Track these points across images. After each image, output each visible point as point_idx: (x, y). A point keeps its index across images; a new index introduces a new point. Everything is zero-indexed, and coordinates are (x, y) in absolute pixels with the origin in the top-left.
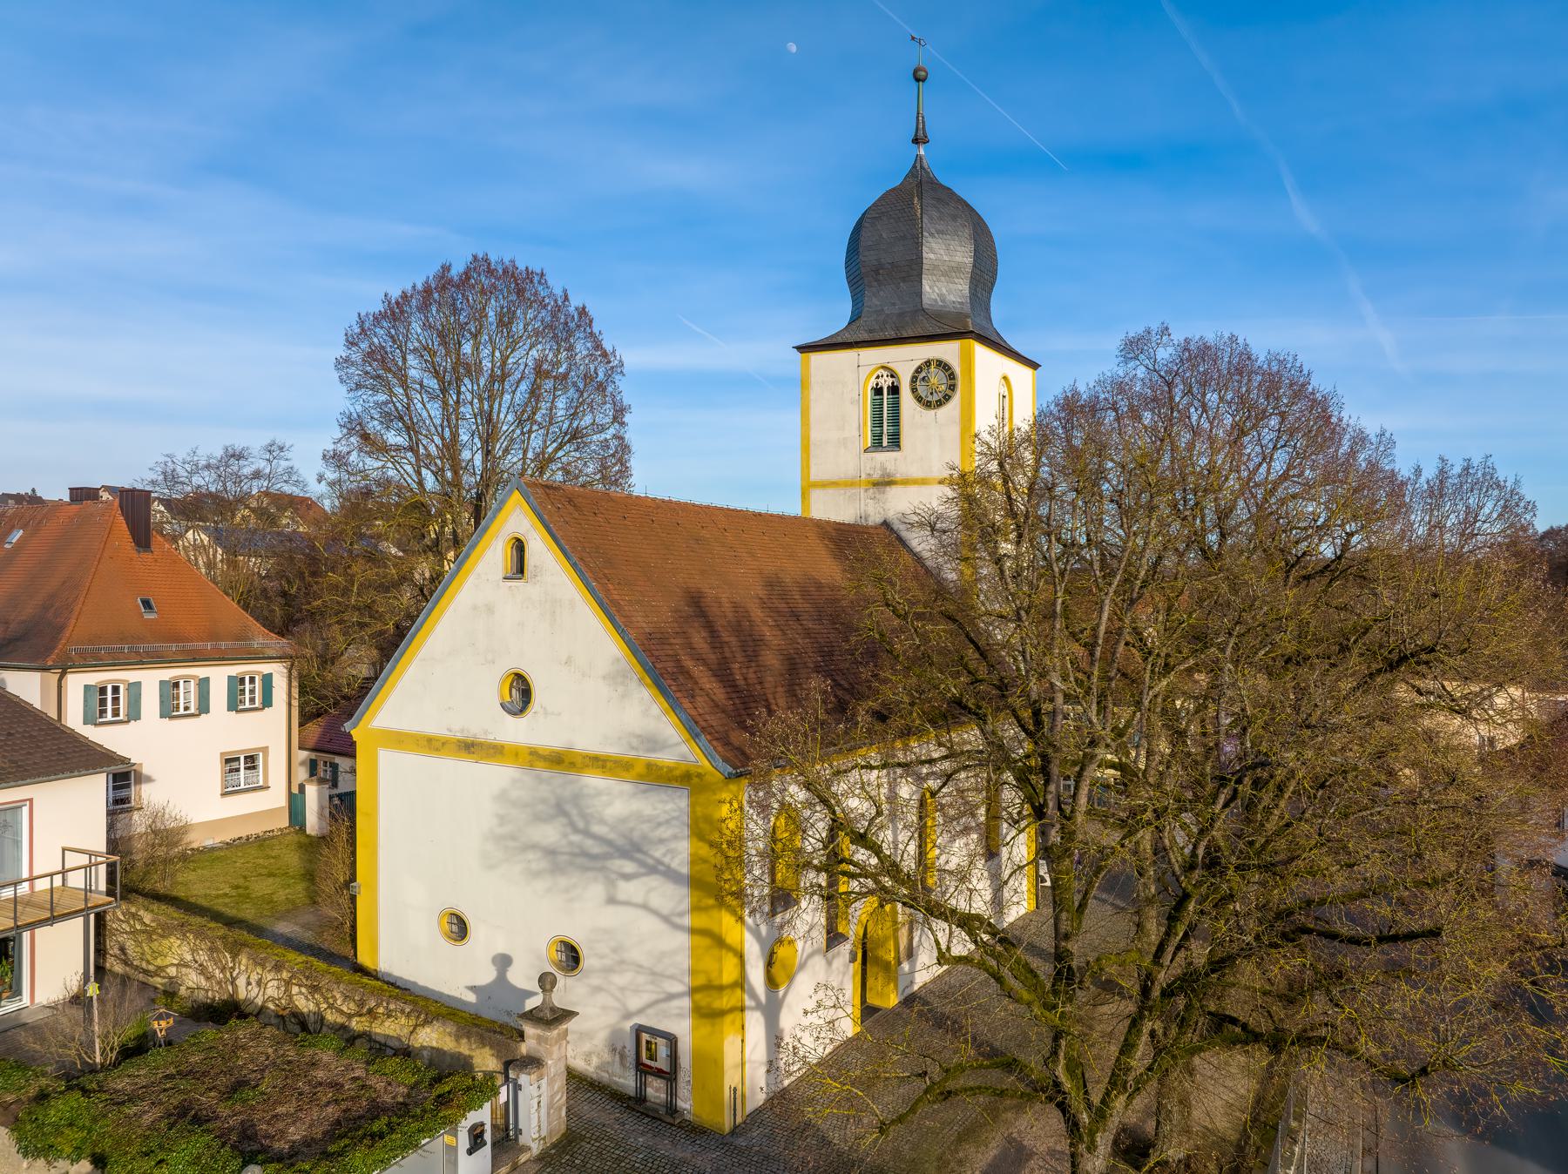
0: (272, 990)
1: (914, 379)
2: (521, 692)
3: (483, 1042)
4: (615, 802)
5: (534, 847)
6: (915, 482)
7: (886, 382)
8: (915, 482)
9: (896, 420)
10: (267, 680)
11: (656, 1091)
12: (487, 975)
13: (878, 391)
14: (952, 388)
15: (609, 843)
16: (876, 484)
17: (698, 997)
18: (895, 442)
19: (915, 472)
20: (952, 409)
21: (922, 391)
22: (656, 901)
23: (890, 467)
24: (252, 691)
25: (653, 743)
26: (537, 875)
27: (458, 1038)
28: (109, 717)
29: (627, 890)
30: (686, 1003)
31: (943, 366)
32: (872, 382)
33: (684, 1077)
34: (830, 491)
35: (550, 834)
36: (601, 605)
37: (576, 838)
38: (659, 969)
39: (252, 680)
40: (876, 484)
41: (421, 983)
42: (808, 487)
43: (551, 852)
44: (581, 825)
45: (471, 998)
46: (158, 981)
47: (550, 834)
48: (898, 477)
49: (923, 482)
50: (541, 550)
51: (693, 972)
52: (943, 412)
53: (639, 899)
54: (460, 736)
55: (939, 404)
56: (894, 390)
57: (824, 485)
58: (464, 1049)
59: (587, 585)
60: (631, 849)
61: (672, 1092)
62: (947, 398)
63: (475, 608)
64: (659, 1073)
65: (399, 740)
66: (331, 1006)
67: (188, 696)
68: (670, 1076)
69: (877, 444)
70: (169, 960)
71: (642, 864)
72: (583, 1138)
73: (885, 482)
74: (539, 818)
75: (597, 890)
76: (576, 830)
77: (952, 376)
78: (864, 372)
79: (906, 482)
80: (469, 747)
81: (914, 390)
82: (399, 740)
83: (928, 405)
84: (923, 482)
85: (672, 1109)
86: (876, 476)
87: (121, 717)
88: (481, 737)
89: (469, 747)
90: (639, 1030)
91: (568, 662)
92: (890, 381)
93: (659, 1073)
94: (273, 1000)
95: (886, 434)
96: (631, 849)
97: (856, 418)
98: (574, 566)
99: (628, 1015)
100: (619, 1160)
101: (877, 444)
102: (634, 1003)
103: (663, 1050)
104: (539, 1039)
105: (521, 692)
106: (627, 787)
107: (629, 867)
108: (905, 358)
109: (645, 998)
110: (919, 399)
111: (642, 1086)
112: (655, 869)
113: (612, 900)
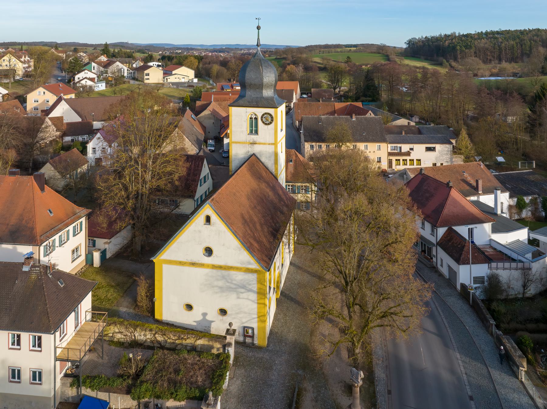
0: (149, 336)
1: (262, 117)
2: (209, 251)
3: (216, 341)
4: (239, 277)
5: (217, 286)
6: (262, 144)
7: (254, 117)
8: (262, 144)
9: (257, 126)
11: (248, 340)
12: (200, 318)
13: (251, 118)
14: (272, 120)
15: (238, 285)
16: (251, 144)
17: (261, 318)
18: (256, 132)
19: (262, 141)
20: (272, 125)
21: (264, 120)
22: (250, 298)
23: (255, 139)
25: (249, 263)
26: (217, 293)
27: (209, 341)
29: (242, 295)
30: (256, 320)
32: (250, 116)
33: (255, 336)
34: (238, 144)
35: (220, 283)
36: (233, 233)
37: (228, 284)
40: (251, 144)
41: (178, 321)
43: (221, 288)
44: (230, 281)
45: (195, 324)
46: (107, 338)
47: (220, 283)
48: (257, 142)
49: (265, 144)
50: (214, 218)
51: (258, 313)
52: (269, 126)
53: (246, 297)
54: (190, 261)
55: (269, 124)
56: (256, 119)
57: (236, 143)
58: (211, 343)
59: (229, 228)
60: (243, 287)
61: (253, 340)
62: (271, 123)
63: (195, 231)
64: (250, 336)
65: (170, 262)
66: (169, 338)
67: (64, 238)
68: (252, 337)
69: (251, 132)
70: (109, 332)
71: (246, 289)
72: (239, 357)
73: (254, 143)
74: (218, 280)
75: (234, 296)
76: (228, 282)
77: (272, 118)
78: (248, 114)
79: (260, 144)
80: (193, 264)
81: (262, 120)
82: (170, 262)
83: (266, 124)
84: (265, 144)
85: (253, 344)
86: (251, 141)
88: (197, 262)
89: (193, 264)
90: (244, 327)
91: (223, 245)
93: (250, 336)
94: (149, 339)
95: (254, 130)
96: (243, 287)
97: (246, 126)
98: (226, 224)
99: (243, 323)
100: (249, 361)
102: (244, 320)
103: (250, 331)
104: (230, 338)
105: (209, 251)
106: (242, 273)
107: (243, 290)
108: (260, 112)
109: (247, 319)
110: (263, 122)
111: (245, 339)
112: (250, 290)
113: (238, 298)
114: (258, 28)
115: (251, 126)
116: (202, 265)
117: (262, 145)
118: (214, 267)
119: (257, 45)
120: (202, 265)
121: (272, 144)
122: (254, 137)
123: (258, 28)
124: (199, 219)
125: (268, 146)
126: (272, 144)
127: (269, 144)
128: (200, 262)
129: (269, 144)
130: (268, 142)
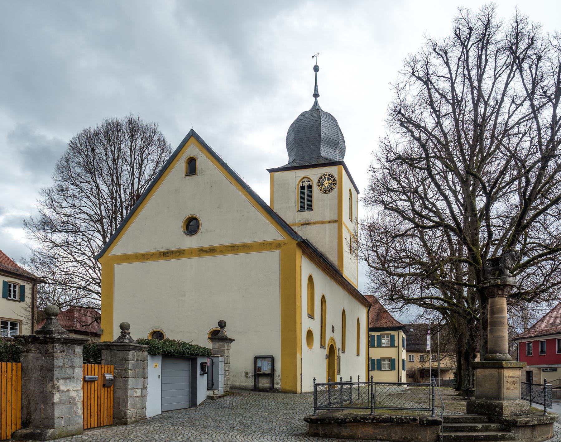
7: (306, 184)
9: (310, 199)
10: (22, 288)
13: (303, 188)
18: (310, 208)
19: (319, 219)
20: (334, 193)
24: (15, 292)
28: (12, 298)
31: (331, 177)
32: (301, 184)
38: (433, 79)
39: (15, 287)
42: (316, 408)
49: (323, 223)
52: (330, 195)
56: (310, 187)
61: (272, 382)
65: (126, 259)
68: (271, 375)
69: (302, 208)
79: (315, 223)
80: (166, 254)
87: (17, 299)
89: (166, 254)
92: (308, 183)
101: (302, 208)
108: (314, 174)
114: (316, 69)
115: (302, 200)
116: (179, 253)
117: (318, 226)
118: (203, 251)
119: (329, 404)
120: (179, 253)
121: (335, 221)
122: (306, 215)
123: (316, 69)
124: (180, 162)
125: (327, 225)
126: (335, 221)
127: (330, 222)
128: (177, 248)
129: (330, 222)
130: (328, 219)
